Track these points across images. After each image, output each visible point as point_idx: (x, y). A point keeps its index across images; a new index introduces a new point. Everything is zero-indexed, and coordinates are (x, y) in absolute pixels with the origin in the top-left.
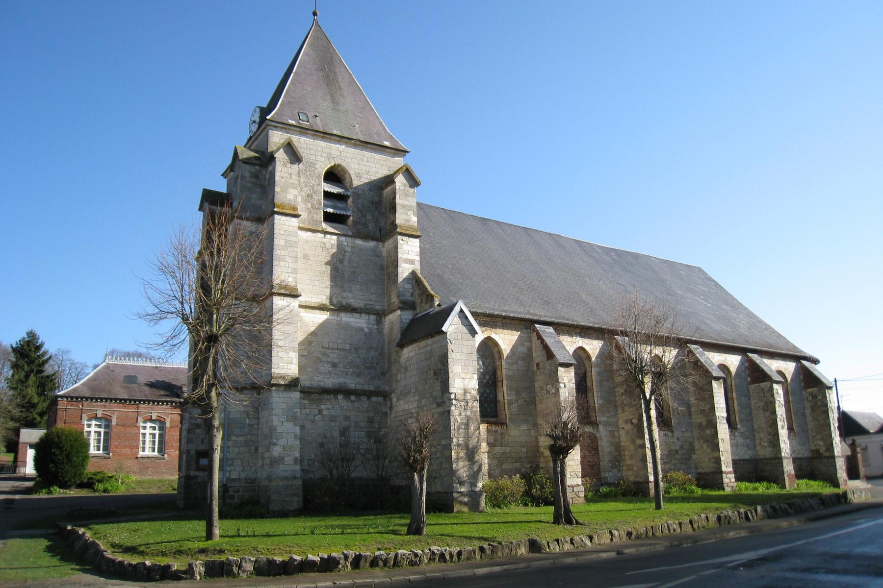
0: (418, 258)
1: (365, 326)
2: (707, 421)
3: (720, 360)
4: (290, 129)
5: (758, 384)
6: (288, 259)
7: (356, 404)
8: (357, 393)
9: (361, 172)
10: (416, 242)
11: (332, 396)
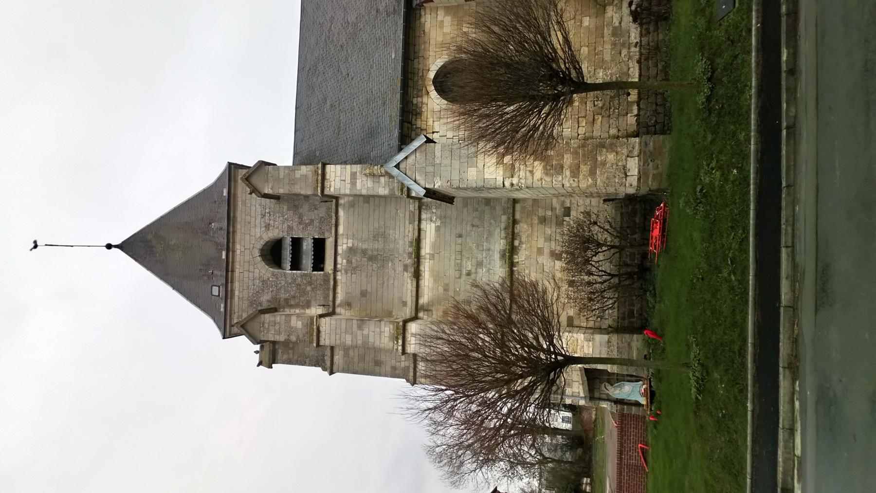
0: (348, 167)
1: (433, 225)
4: (231, 310)
6: (365, 332)
7: (524, 239)
8: (512, 236)
9: (263, 225)
10: (330, 169)
11: (515, 269)
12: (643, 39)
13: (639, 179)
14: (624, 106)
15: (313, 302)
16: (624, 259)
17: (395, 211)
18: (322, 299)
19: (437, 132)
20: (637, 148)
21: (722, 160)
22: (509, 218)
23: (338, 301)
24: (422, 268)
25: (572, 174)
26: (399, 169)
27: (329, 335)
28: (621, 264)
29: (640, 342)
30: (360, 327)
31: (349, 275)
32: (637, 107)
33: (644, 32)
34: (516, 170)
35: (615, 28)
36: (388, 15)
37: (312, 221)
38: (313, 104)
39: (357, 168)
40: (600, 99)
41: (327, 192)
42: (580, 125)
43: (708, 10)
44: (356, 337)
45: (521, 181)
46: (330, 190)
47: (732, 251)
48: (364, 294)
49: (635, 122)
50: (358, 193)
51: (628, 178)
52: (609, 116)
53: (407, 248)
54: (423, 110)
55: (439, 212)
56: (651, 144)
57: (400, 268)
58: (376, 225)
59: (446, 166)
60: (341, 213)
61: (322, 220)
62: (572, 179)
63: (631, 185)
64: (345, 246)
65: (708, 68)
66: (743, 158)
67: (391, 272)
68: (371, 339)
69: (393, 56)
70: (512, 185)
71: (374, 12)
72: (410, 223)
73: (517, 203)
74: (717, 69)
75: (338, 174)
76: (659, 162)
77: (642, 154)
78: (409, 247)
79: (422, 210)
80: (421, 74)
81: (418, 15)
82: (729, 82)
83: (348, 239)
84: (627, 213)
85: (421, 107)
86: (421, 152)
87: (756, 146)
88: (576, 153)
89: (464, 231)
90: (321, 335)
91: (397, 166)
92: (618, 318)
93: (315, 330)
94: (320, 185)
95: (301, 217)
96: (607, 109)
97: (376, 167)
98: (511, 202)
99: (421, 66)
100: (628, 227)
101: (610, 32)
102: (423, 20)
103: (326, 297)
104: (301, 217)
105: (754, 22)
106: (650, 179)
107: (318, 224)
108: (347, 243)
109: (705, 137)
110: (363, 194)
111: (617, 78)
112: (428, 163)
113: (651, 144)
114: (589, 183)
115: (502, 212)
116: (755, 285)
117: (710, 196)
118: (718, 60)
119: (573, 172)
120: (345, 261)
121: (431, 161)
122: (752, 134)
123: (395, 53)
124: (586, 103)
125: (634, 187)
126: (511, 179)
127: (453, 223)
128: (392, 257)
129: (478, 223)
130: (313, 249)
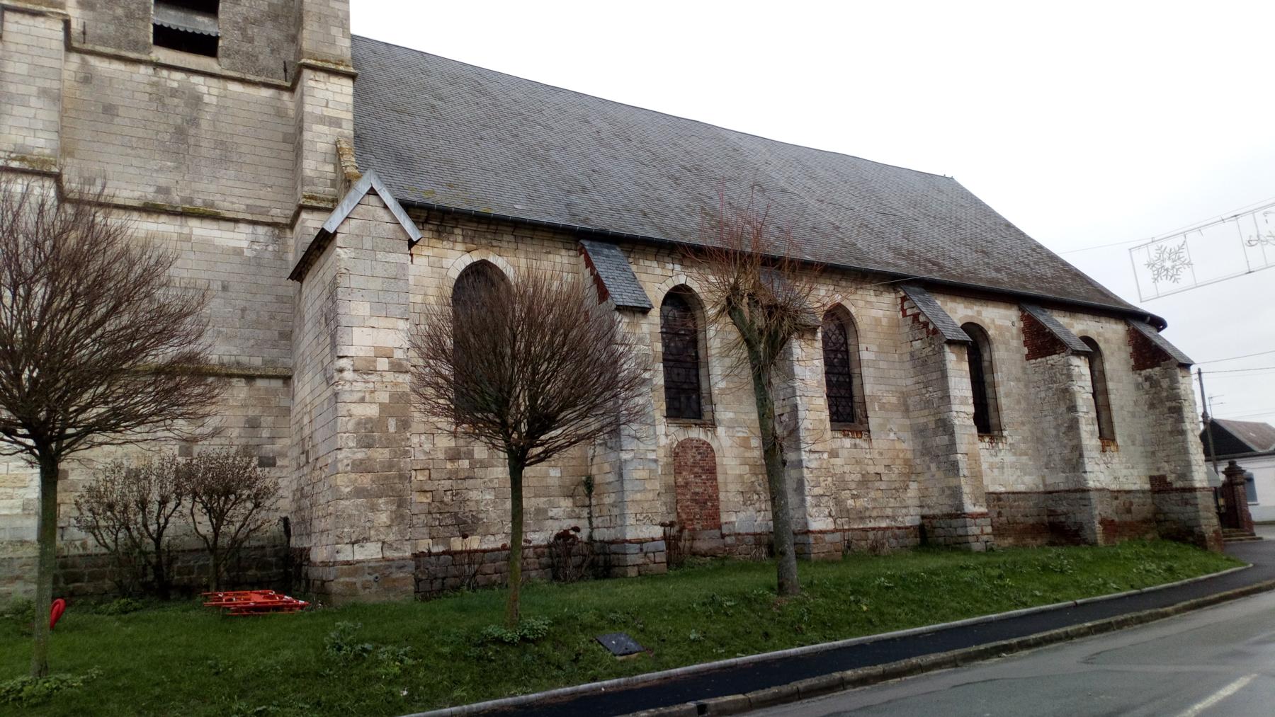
0: (350, 116)
1: (245, 244)
2: (937, 421)
3: (967, 316)
5: (1043, 359)
10: (347, 86)
12: (531, 549)
13: (348, 563)
14: (443, 532)
15: (90, 14)
16: (180, 557)
17: (269, 184)
18: (99, 31)
19: (412, 261)
20: (396, 555)
21: (418, 672)
22: (257, 369)
23: (93, 61)
24: (163, 218)
25: (357, 462)
26: (368, 193)
27: (28, 32)
28: (171, 554)
29: (26, 597)
30: (44, 93)
31: (148, 89)
32: (441, 551)
33: (539, 550)
34: (365, 376)
35: (546, 511)
36: (567, 205)
37: (251, 40)
38: (430, 79)
39: (348, 129)
40: (454, 498)
41: (307, 73)
42: (418, 472)
43: (603, 623)
44: (24, 83)
45: (348, 384)
46: (311, 79)
47: (278, 709)
48: (109, 110)
49: (420, 550)
50: (306, 125)
51: (349, 546)
52: (430, 513)
53: (200, 196)
54: (445, 243)
55: (267, 255)
56: (402, 575)
57: (163, 180)
58: (243, 149)
59: (373, 268)
60: (266, 93)
61: (251, 58)
62: (349, 461)
63: (337, 552)
64: (204, 89)
65: (538, 634)
66: (427, 701)
67: (153, 165)
68: (18, 110)
69: (517, 206)
70: (341, 371)
71: (566, 187)
72: (247, 206)
73: (284, 383)
74: (537, 646)
75: (338, 98)
76: (373, 589)
77: (387, 563)
78: (204, 201)
79: (271, 229)
80: (494, 243)
81: (568, 246)
82: (526, 664)
83: (217, 96)
84: (265, 555)
85: (448, 240)
86: (395, 231)
87: (450, 714)
88: (390, 466)
89: (234, 295)
90: (27, 17)
91: (372, 192)
92: (65, 557)
93: (37, 8)
94: (319, 64)
95: (256, 22)
96: (440, 509)
97: (353, 159)
98: (285, 372)
99: (505, 244)
100: (239, 559)
101: (541, 506)
102: (563, 252)
103: (102, 40)
104: (256, 22)
105: (606, 683)
106: (347, 579)
107: (244, 49)
108: (209, 94)
109: (443, 644)
110: (304, 133)
111: (482, 519)
112: (378, 240)
113: (402, 575)
114: (343, 489)
115: (268, 358)
116: (689, 674)
117: (358, 665)
118: (549, 646)
119: (361, 463)
120: (175, 85)
121: (380, 245)
122: (466, 707)
123: (520, 209)
124: (449, 479)
125: (335, 558)
126: (351, 369)
127: (249, 278)
128: (185, 168)
129: (248, 318)
130: (198, 32)
